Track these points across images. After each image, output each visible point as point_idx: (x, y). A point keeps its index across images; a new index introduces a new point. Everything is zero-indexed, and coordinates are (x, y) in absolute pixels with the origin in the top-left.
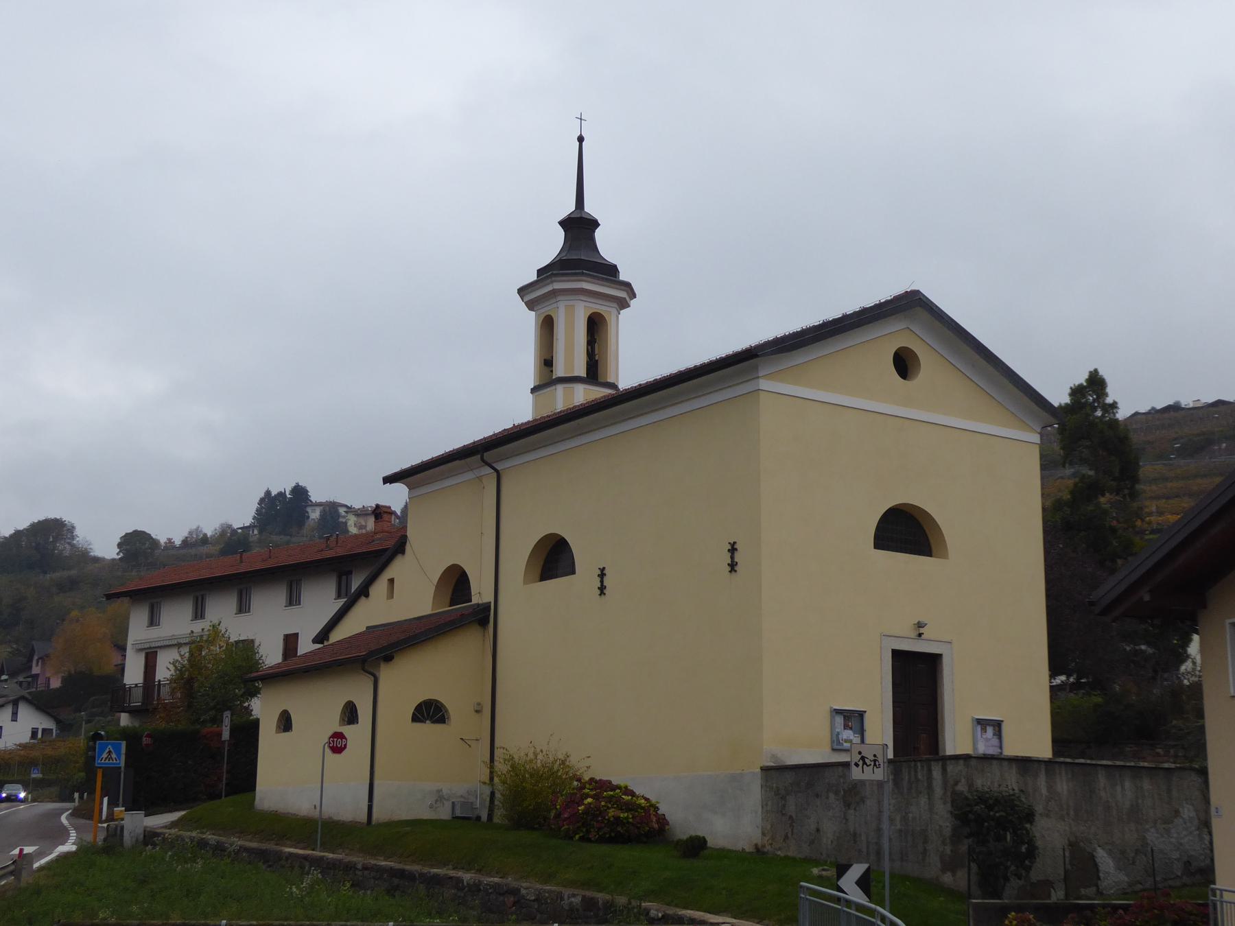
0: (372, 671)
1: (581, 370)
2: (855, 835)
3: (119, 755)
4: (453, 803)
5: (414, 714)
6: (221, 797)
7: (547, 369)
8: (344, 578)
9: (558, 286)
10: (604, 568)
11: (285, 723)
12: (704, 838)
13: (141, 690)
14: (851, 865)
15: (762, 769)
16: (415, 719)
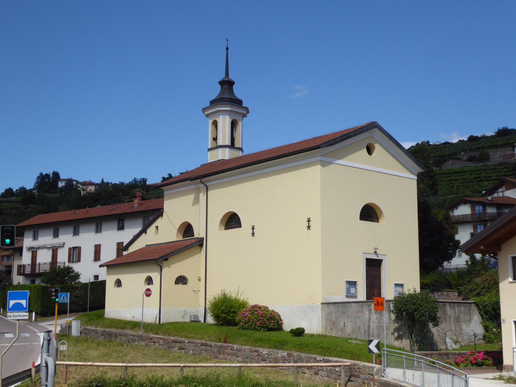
0: (159, 264)
1: (228, 142)
2: (359, 328)
3: (67, 298)
4: (191, 315)
5: (175, 281)
7: (215, 142)
8: (121, 222)
10: (254, 226)
11: (118, 283)
12: (303, 328)
13: (30, 267)
15: (322, 304)
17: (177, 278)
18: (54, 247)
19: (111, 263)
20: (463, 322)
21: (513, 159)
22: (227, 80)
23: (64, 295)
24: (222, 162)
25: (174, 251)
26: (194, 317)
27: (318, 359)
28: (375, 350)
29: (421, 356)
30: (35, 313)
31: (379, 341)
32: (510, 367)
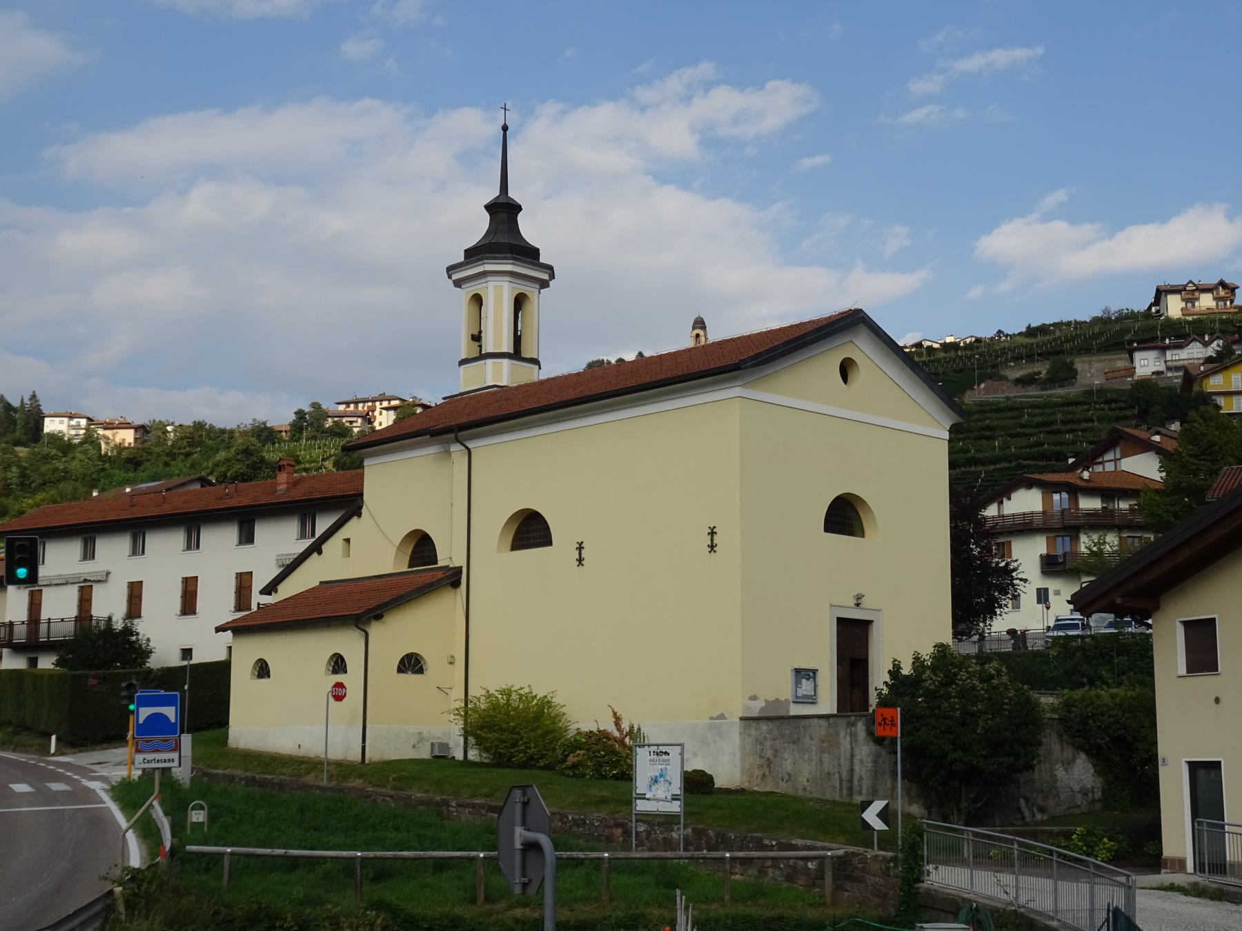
4: (432, 744)
5: (399, 666)
9: (489, 267)
11: (262, 670)
14: (873, 801)
15: (741, 719)
16: (400, 670)
17: (403, 658)
18: (85, 581)
19: (242, 624)
20: (1058, 763)
21: (1130, 379)
22: (505, 201)
24: (493, 393)
25: (395, 596)
26: (439, 745)
27: (766, 842)
28: (878, 825)
29: (1012, 837)
30: (58, 740)
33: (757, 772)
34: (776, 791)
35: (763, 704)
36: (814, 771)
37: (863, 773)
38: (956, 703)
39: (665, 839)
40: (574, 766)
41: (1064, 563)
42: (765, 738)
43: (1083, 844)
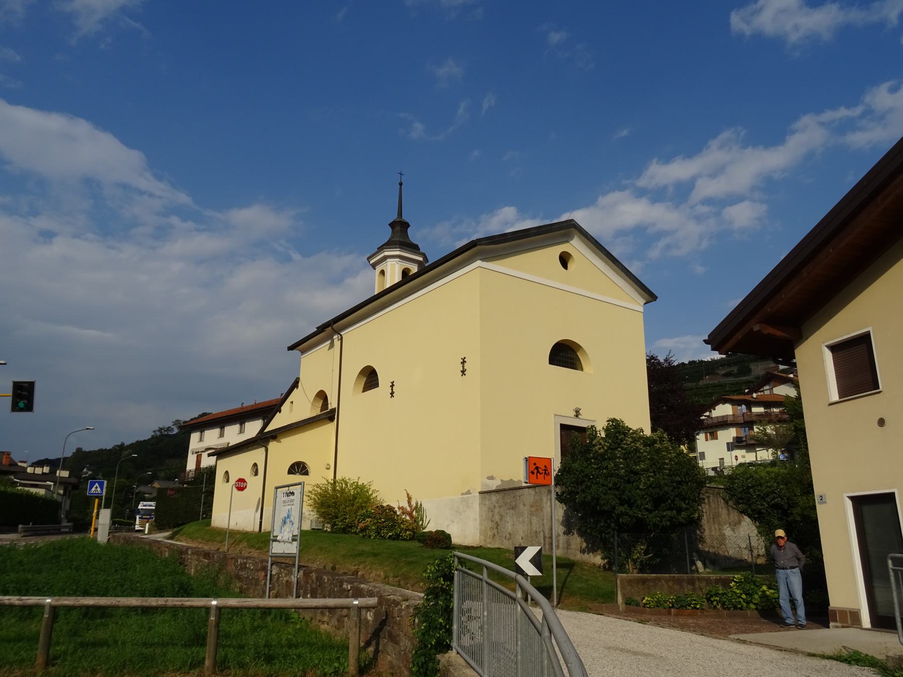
2: (536, 532)
6: (198, 519)
15: (480, 493)
20: (726, 524)
23: (97, 484)
28: (532, 570)
31: (541, 550)
32: (848, 612)
33: (490, 533)
34: (502, 547)
35: (499, 483)
36: (526, 530)
37: (559, 531)
38: (621, 463)
39: (287, 581)
40: (363, 530)
41: (746, 441)
42: (495, 506)
43: (741, 592)
